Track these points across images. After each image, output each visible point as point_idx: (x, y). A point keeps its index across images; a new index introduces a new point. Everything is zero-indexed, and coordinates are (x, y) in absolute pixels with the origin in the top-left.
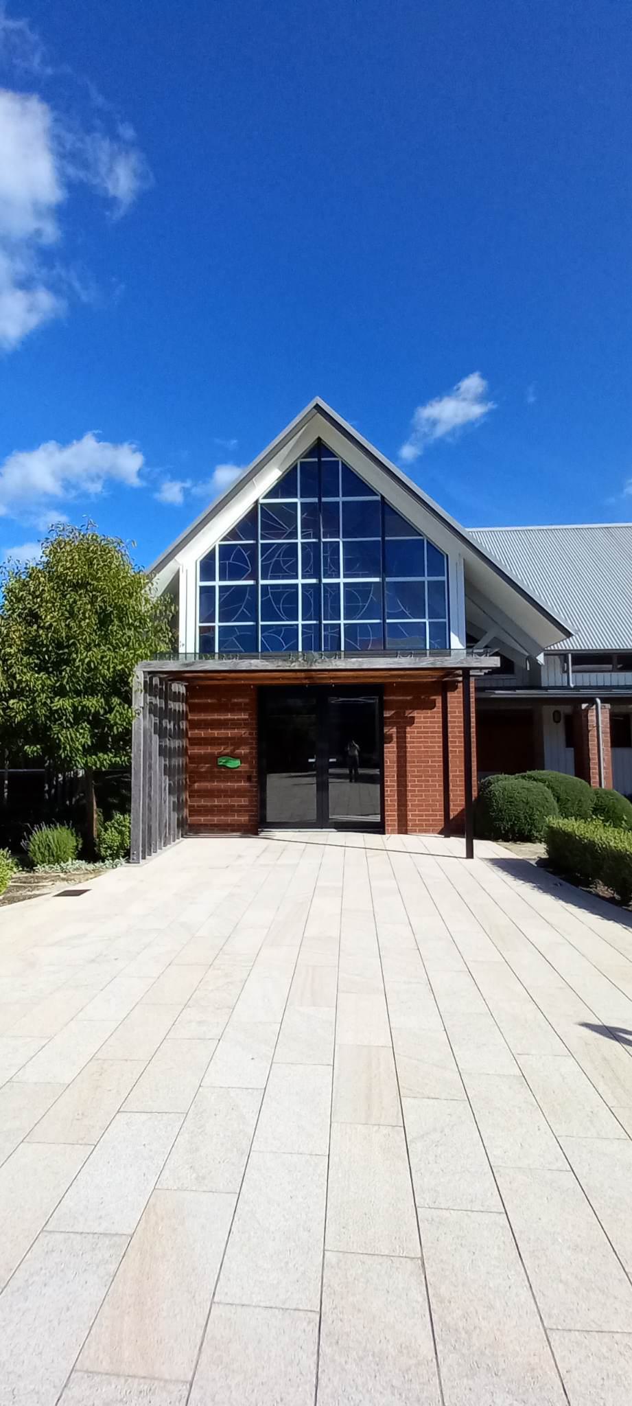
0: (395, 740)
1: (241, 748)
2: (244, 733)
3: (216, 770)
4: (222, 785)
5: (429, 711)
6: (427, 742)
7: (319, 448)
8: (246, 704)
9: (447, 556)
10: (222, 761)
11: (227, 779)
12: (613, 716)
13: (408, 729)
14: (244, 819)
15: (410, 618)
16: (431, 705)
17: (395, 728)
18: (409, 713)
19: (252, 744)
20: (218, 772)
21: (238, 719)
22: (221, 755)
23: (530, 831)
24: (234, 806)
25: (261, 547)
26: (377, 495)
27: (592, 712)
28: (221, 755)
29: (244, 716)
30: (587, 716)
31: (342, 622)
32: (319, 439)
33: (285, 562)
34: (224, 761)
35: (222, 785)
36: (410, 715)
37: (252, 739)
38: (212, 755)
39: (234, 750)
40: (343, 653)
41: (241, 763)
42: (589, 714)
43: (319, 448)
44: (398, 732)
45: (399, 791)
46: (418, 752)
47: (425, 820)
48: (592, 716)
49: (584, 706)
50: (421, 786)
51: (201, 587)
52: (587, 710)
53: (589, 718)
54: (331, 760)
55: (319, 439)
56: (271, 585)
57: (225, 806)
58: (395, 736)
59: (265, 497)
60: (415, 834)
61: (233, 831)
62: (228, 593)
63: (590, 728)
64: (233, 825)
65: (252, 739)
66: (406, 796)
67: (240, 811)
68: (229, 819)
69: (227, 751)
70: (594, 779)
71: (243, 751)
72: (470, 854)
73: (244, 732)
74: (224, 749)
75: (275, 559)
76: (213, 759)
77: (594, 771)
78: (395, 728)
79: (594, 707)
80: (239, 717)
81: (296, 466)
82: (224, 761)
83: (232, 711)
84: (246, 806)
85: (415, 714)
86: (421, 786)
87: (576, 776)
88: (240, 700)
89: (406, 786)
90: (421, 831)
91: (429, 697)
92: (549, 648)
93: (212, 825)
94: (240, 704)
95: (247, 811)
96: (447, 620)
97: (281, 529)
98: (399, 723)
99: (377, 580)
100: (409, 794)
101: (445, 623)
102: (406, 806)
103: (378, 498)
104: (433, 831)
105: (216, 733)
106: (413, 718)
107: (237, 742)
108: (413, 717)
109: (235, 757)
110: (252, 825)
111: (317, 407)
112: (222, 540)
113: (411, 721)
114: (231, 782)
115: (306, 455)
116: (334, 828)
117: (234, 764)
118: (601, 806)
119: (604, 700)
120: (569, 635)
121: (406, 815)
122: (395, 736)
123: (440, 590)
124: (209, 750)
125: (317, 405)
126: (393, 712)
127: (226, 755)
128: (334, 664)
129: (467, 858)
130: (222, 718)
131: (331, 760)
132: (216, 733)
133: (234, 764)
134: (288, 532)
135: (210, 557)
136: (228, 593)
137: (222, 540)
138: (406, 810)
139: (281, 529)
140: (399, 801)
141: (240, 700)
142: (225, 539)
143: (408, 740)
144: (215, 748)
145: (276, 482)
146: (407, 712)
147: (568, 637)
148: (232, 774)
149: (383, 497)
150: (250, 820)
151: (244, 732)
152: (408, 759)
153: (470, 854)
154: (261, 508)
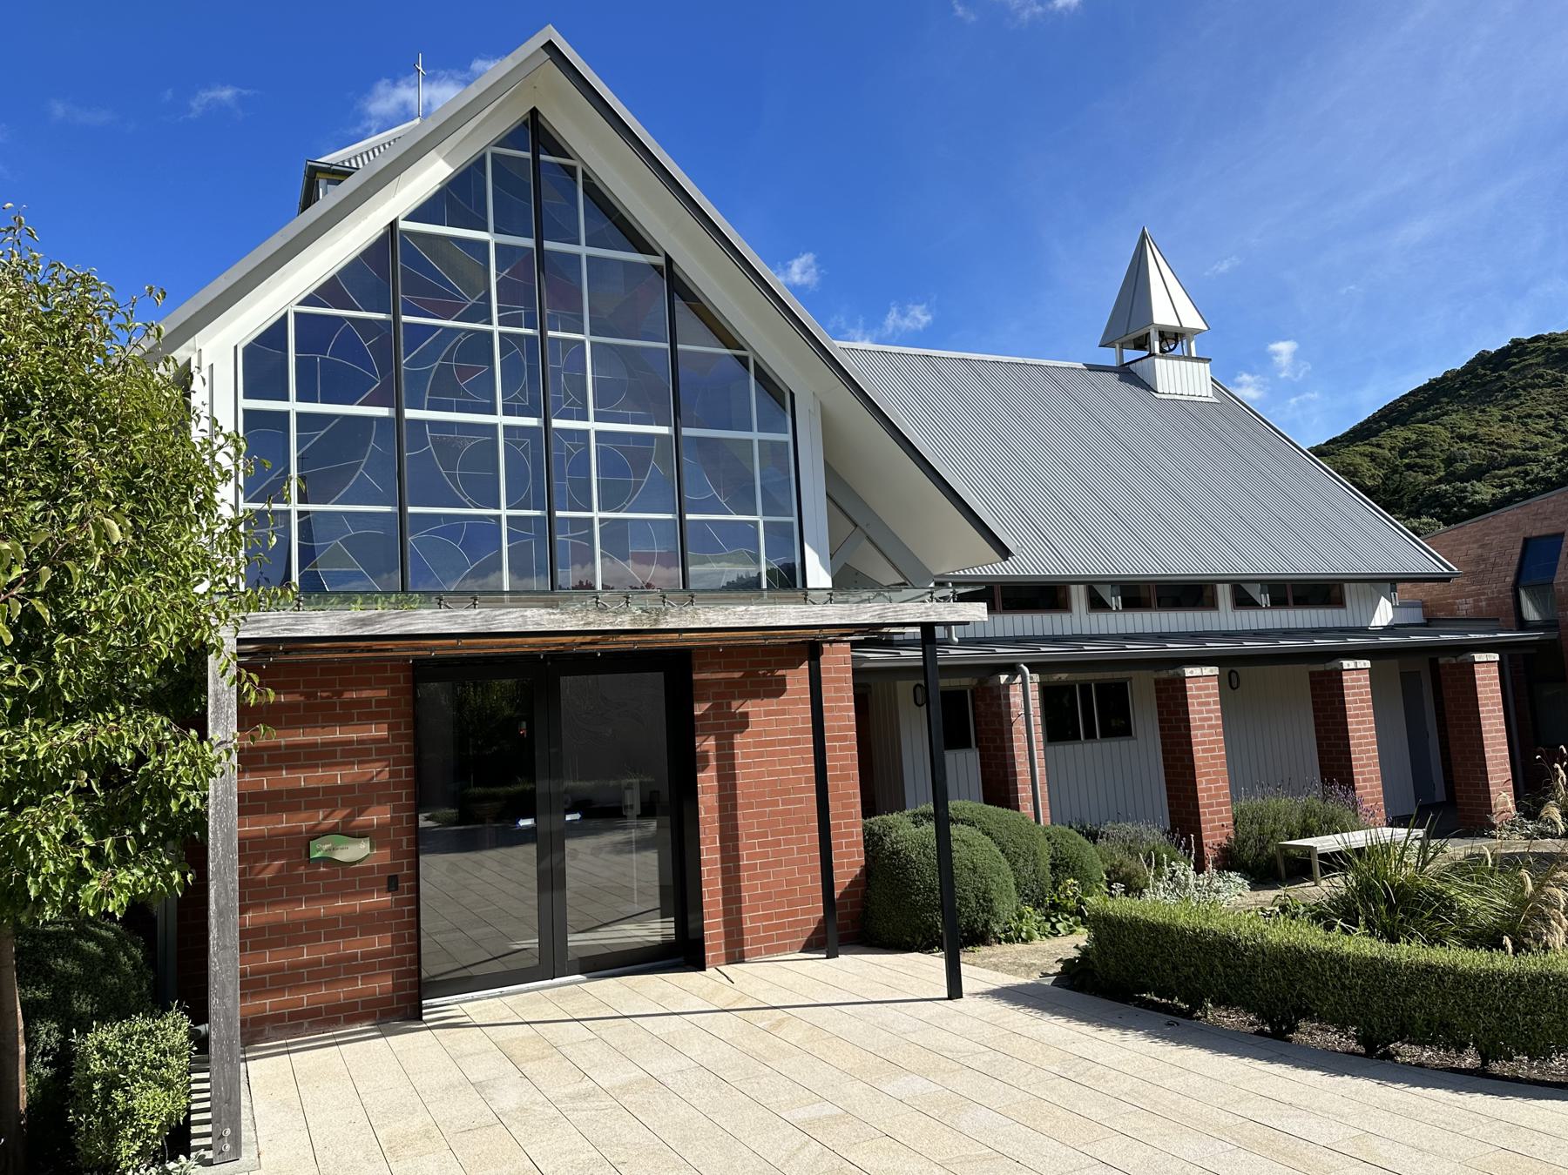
0: (713, 763)
1: (371, 810)
2: (378, 773)
3: (302, 870)
4: (322, 909)
5: (775, 700)
6: (773, 763)
7: (534, 131)
8: (380, 702)
9: (792, 395)
10: (319, 849)
11: (334, 892)
12: (1046, 691)
13: (738, 739)
14: (382, 984)
15: (729, 513)
16: (777, 689)
17: (712, 738)
18: (738, 706)
19: (399, 797)
20: (309, 877)
21: (360, 742)
22: (316, 834)
23: (987, 922)
24: (354, 957)
25: (786, 427)
26: (656, 254)
27: (1016, 690)
28: (316, 834)
29: (378, 731)
30: (1007, 697)
31: (596, 514)
32: (534, 112)
33: (464, 373)
34: (326, 847)
35: (322, 909)
36: (740, 710)
37: (397, 786)
38: (291, 834)
39: (352, 816)
40: (275, 506)
41: (372, 848)
42: (1011, 693)
43: (534, 131)
44: (718, 747)
45: (724, 870)
46: (758, 785)
47: (777, 927)
48: (1016, 698)
49: (1003, 678)
50: (766, 855)
51: (246, 411)
52: (1007, 686)
53: (1012, 700)
54: (568, 818)
55: (534, 112)
56: (432, 423)
57: (329, 961)
58: (712, 754)
59: (409, 218)
60: (758, 958)
61: (351, 1020)
62: (322, 432)
63: (1013, 719)
64: (354, 1006)
65: (397, 786)
66: (738, 879)
67: (372, 967)
68: (342, 992)
69: (331, 821)
70: (1027, 808)
71: (377, 816)
72: (955, 990)
73: (377, 771)
74: (324, 819)
75: (439, 362)
76: (300, 844)
77: (1024, 794)
78: (712, 738)
79: (1019, 679)
80: (365, 735)
81: (484, 157)
82: (326, 847)
83: (344, 720)
84: (389, 952)
85: (750, 707)
86: (766, 855)
87: (987, 801)
88: (366, 694)
89: (737, 858)
90: (770, 950)
91: (772, 671)
92: (962, 573)
93: (294, 1016)
94: (366, 703)
95: (383, 965)
96: (795, 520)
97: (452, 297)
98: (721, 726)
99: (664, 430)
100: (744, 874)
101: (792, 523)
102: (739, 900)
103: (660, 261)
104: (791, 949)
105: (303, 779)
106: (746, 715)
107: (359, 796)
108: (746, 715)
109: (353, 833)
110: (400, 999)
111: (550, 46)
112: (301, 304)
113: (742, 722)
114: (345, 896)
115: (501, 141)
116: (581, 974)
117: (355, 851)
118: (1063, 859)
119: (1033, 668)
120: (1005, 553)
121: (740, 921)
122: (712, 754)
123: (784, 460)
124: (285, 822)
125: (550, 42)
126: (707, 705)
127: (333, 831)
128: (703, 617)
129: (950, 998)
130: (319, 739)
131: (568, 818)
132: (303, 779)
133: (355, 851)
134: (470, 304)
135: (274, 335)
136: (322, 432)
137: (301, 304)
138: (739, 911)
139: (452, 297)
140: (725, 891)
141: (366, 694)
142: (306, 301)
143: (738, 761)
144: (303, 815)
145: (438, 187)
146: (735, 704)
147: (1005, 559)
148: (348, 878)
149: (669, 260)
150: (396, 987)
151: (377, 771)
152: (740, 801)
153: (955, 990)
154: (401, 236)
